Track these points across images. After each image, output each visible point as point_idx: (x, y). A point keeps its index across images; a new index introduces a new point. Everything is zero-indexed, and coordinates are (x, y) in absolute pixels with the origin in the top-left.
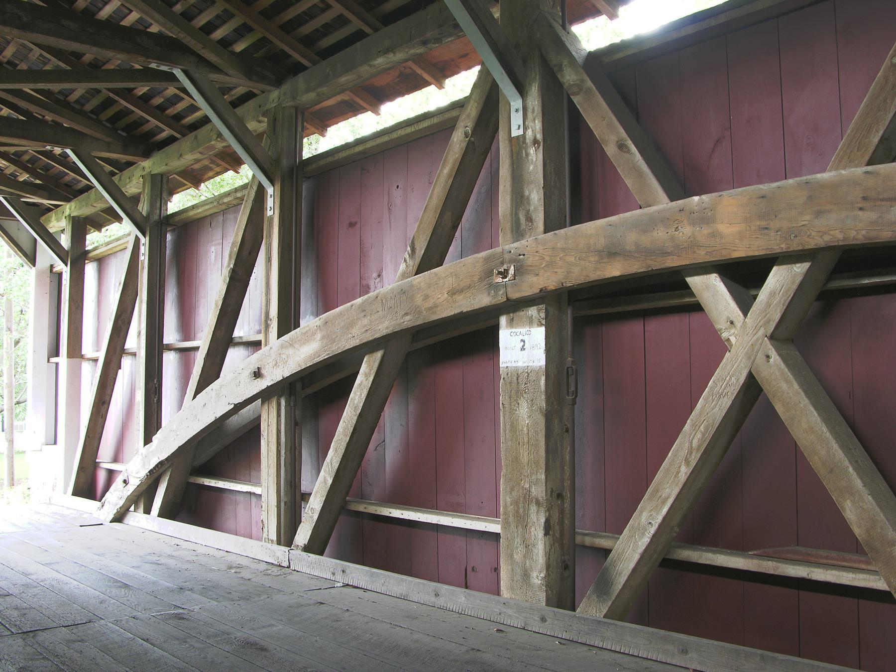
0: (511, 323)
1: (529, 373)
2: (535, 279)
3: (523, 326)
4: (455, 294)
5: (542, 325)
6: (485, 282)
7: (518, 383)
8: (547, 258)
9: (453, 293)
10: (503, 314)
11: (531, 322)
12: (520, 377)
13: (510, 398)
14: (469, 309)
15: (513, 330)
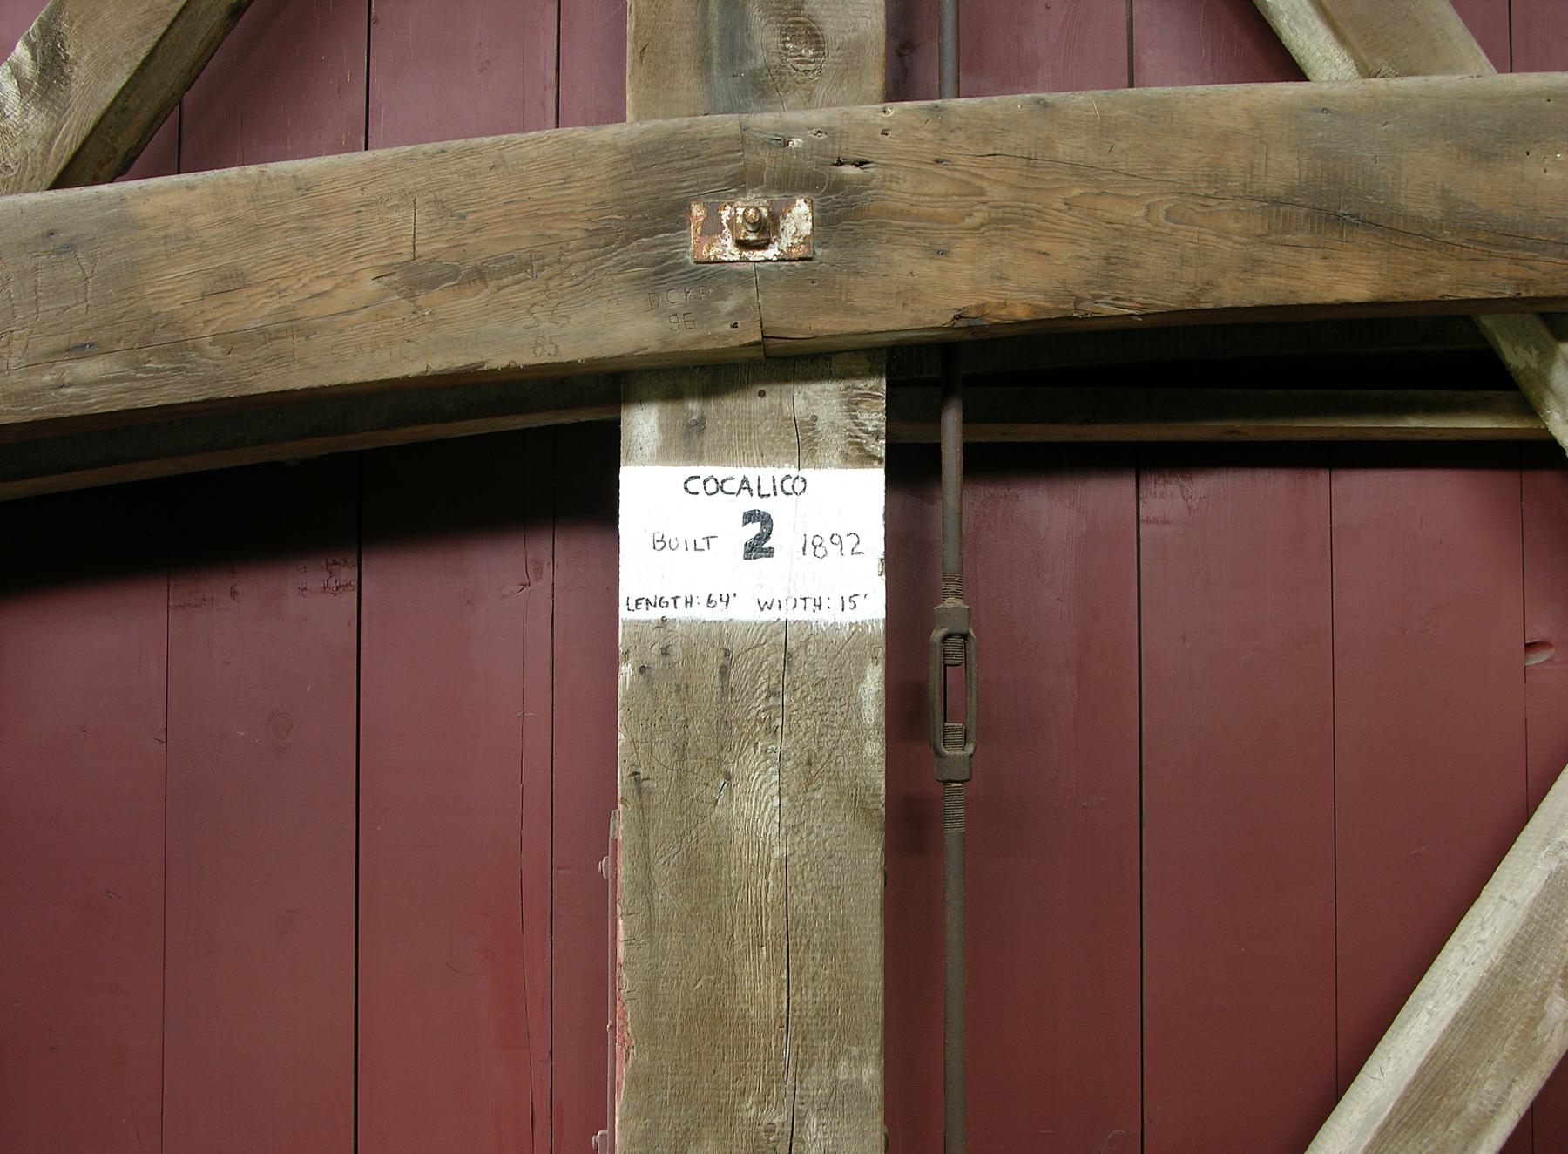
0: (687, 444)
1: (789, 649)
2: (928, 270)
3: (764, 453)
4: (432, 284)
5: (866, 459)
6: (632, 252)
7: (726, 690)
8: (997, 194)
9: (417, 278)
10: (641, 399)
11: (804, 443)
12: (729, 675)
13: (681, 750)
14: (525, 359)
15: (704, 471)
